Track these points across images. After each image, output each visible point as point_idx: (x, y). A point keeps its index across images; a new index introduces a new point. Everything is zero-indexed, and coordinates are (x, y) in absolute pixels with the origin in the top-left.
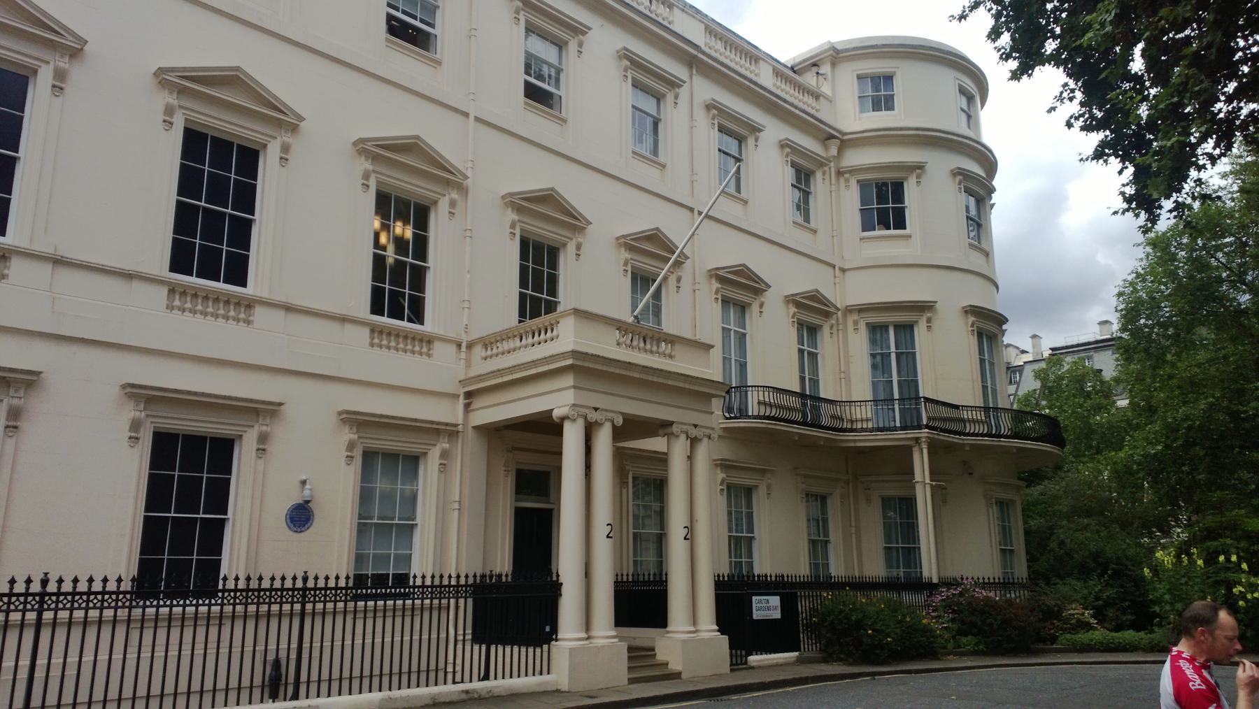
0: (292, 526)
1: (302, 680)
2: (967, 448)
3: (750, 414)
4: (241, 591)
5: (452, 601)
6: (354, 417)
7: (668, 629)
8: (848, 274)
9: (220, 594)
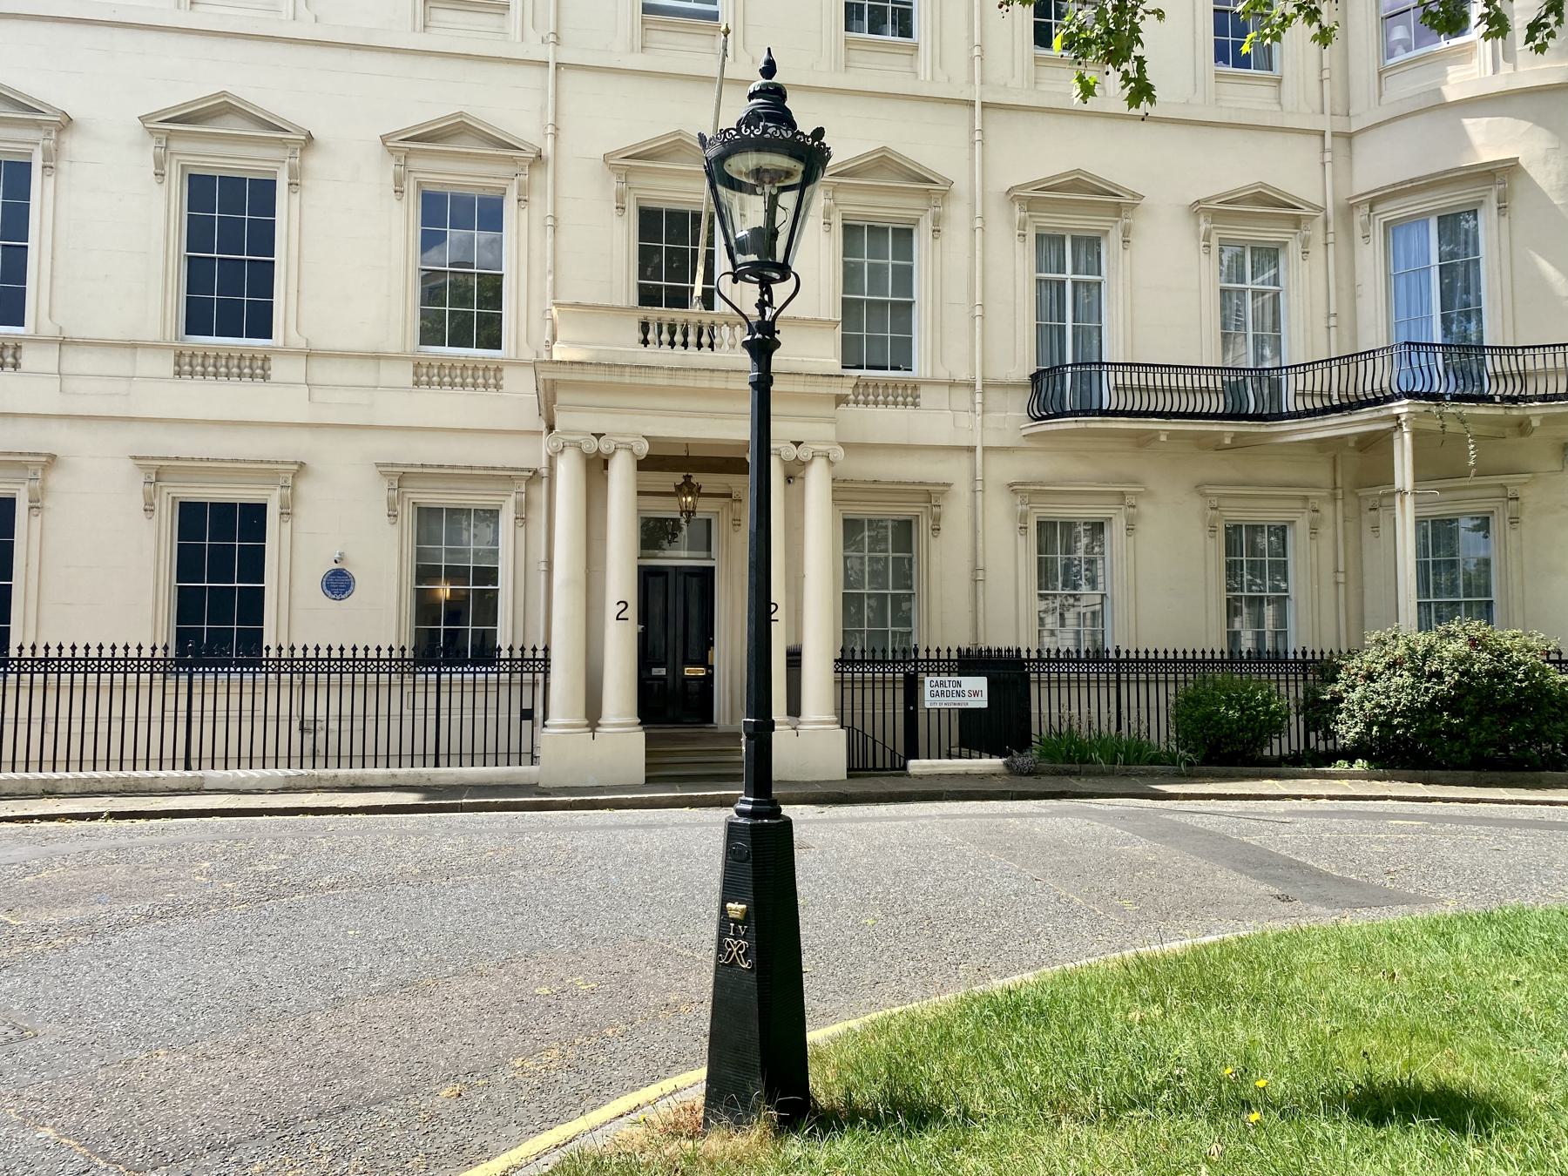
1: (192, 756)
6: (390, 469)
7: (801, 719)
9: (264, 663)
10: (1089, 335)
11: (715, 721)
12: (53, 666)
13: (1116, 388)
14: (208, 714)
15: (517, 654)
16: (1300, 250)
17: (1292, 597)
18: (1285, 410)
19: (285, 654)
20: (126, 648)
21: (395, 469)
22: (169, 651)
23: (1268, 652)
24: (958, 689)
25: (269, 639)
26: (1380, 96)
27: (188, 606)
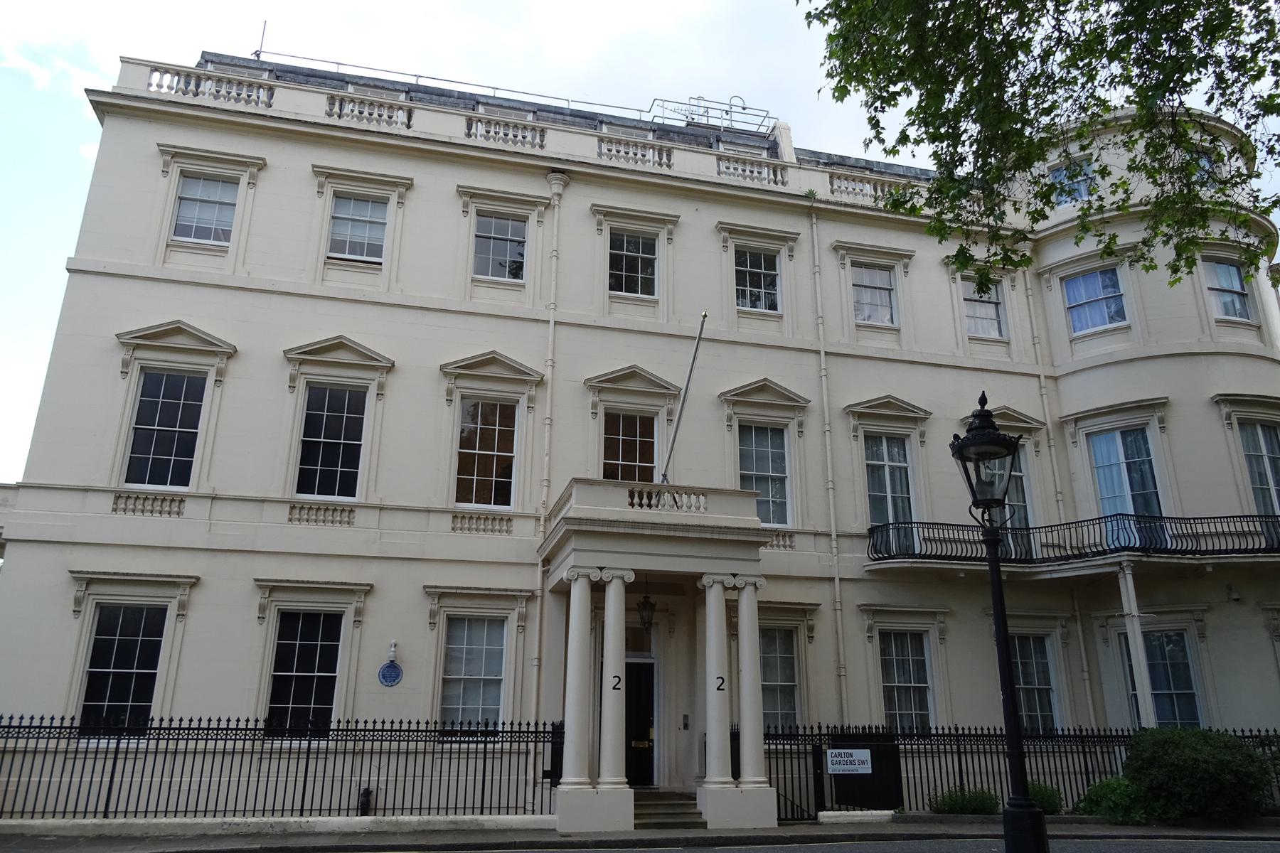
0: (384, 681)
2: (1209, 569)
3: (917, 551)
4: (251, 729)
5: (531, 745)
6: (434, 590)
8: (1063, 384)
10: (903, 505)
11: (655, 783)
12: (174, 734)
13: (924, 539)
14: (320, 774)
15: (516, 728)
16: (1034, 449)
17: (1054, 688)
18: (1035, 557)
19: (165, 724)
20: (418, 723)
21: (437, 590)
22: (249, 723)
23: (1026, 729)
24: (851, 759)
25: (155, 713)
26: (1073, 355)
27: (279, 689)
